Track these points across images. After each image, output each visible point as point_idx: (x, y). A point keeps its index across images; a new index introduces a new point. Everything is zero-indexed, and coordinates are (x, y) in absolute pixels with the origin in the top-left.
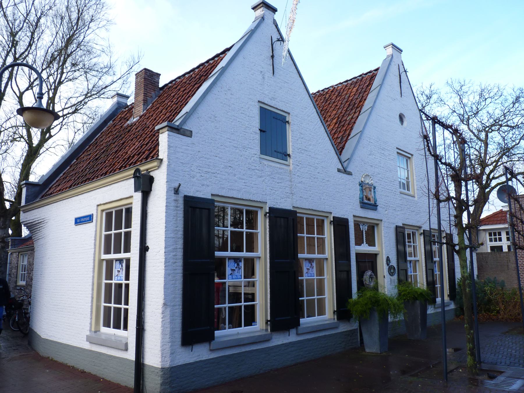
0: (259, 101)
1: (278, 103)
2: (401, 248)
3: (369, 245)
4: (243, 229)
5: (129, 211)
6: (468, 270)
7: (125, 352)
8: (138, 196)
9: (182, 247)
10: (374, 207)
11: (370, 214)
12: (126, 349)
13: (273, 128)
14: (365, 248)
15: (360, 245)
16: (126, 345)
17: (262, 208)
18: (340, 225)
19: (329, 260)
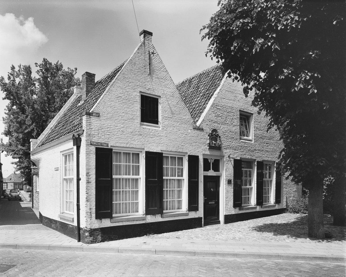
0: (140, 92)
1: (153, 89)
2: (239, 182)
3: (215, 171)
4: (130, 163)
5: (73, 154)
6: (303, 262)
7: (98, 118)
8: (75, 147)
9: (95, 185)
10: (219, 148)
11: (216, 153)
12: (73, 221)
13: (149, 109)
14: (211, 173)
15: (208, 171)
16: (73, 219)
17: (142, 152)
18: (193, 160)
19: (185, 180)
